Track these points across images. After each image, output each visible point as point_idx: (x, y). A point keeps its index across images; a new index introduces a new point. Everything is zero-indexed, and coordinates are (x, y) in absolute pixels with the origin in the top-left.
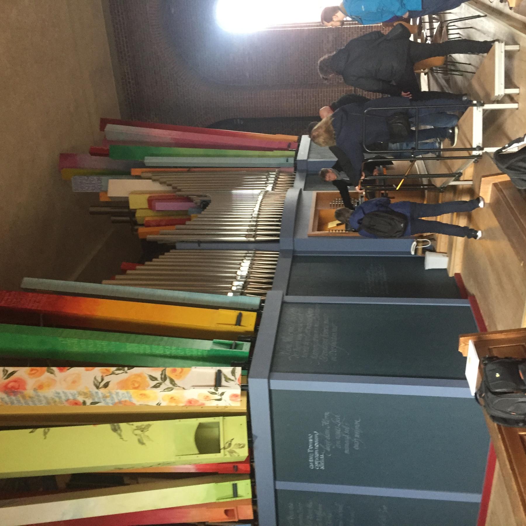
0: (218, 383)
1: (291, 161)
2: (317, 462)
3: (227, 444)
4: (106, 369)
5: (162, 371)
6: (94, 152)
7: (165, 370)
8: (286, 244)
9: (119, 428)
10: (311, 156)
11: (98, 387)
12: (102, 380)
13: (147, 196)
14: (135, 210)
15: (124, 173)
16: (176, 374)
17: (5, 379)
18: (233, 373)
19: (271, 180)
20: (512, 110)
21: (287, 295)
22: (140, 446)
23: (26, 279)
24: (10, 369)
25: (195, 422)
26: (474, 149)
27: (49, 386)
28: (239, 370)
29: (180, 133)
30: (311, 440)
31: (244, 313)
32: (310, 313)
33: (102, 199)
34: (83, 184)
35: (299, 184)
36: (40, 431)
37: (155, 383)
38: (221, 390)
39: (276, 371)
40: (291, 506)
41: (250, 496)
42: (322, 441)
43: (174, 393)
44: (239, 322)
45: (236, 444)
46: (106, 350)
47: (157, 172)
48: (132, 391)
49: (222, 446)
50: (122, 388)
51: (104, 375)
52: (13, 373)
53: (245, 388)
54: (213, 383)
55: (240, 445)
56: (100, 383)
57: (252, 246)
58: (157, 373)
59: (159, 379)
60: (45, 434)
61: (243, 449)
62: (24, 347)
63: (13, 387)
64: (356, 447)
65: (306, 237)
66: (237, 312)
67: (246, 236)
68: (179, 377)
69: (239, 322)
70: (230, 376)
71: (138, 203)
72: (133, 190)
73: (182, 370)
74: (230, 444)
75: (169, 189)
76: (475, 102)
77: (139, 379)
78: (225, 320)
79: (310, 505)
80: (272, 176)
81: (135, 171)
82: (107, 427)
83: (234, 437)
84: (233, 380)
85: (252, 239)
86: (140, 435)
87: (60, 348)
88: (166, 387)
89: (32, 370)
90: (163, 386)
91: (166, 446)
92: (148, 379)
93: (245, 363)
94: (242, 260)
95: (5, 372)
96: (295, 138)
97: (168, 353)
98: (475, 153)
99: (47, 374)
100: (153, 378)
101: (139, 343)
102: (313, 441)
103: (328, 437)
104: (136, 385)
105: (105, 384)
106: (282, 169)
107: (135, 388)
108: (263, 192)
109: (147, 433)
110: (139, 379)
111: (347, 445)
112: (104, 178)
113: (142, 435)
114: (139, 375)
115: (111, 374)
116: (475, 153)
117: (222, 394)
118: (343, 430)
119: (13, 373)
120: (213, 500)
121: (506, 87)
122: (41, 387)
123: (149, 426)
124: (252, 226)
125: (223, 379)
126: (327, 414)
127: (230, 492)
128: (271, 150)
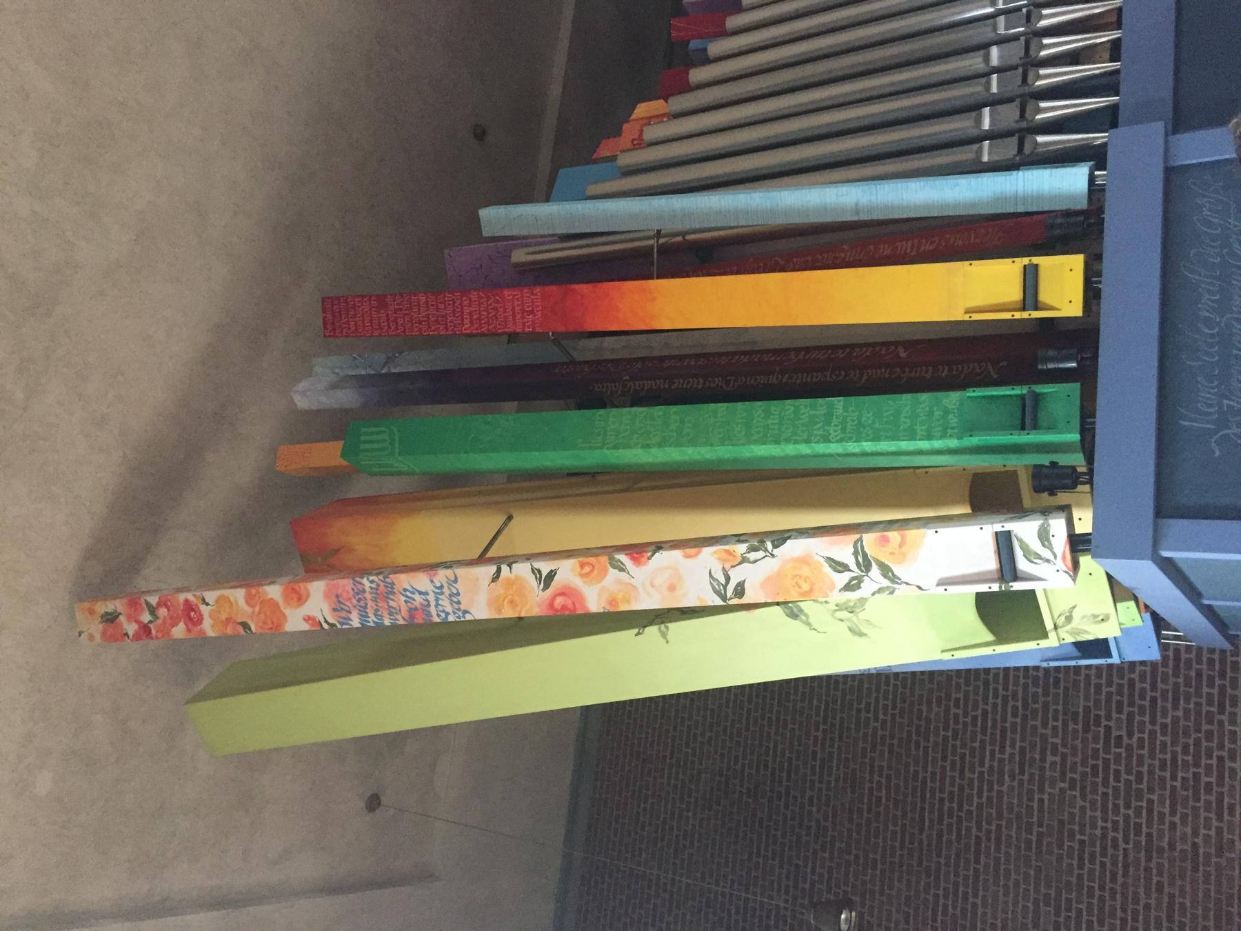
3: (1063, 619)
4: (727, 551)
5: (855, 546)
7: (861, 540)
9: (801, 611)
12: (728, 579)
16: (889, 549)
17: (544, 590)
18: (1044, 536)
21: (1175, 131)
22: (856, 638)
23: (486, 213)
37: (847, 576)
44: (1030, 296)
45: (1084, 617)
51: (727, 566)
52: (551, 575)
55: (1095, 616)
56: (725, 587)
58: (843, 549)
59: (853, 566)
60: (664, 635)
61: (1104, 624)
68: (902, 557)
73: (903, 538)
74: (1069, 619)
77: (805, 571)
84: (1048, 561)
86: (850, 620)
88: (876, 587)
92: (827, 569)
95: (537, 572)
99: (613, 573)
100: (840, 567)
104: (806, 587)
105: (736, 589)
109: (862, 615)
110: (805, 571)
113: (854, 619)
114: (804, 560)
115: (740, 563)
119: (551, 575)
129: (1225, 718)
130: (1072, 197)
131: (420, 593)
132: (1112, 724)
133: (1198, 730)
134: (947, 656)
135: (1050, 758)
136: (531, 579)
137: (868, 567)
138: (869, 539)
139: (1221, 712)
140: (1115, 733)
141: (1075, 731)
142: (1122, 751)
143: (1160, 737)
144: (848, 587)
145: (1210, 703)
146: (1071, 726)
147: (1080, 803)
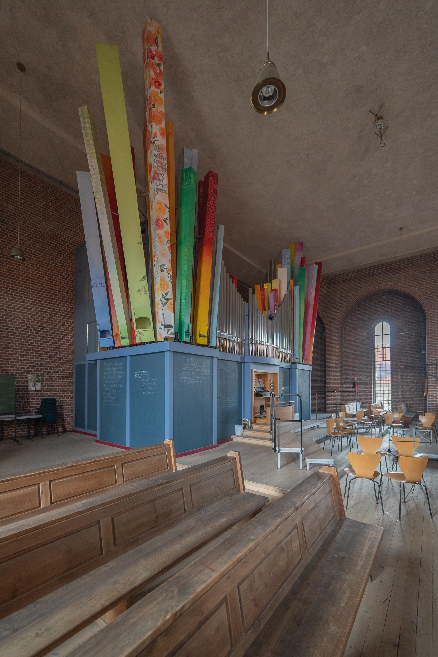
0: (165, 326)
1: (297, 361)
2: (138, 375)
6: (303, 260)
8: (248, 359)
10: (300, 371)
11: (161, 266)
12: (165, 269)
13: (278, 288)
14: (271, 283)
15: (292, 276)
18: (171, 333)
19: (286, 351)
20: (299, 466)
22: (137, 290)
23: (223, 226)
24: (168, 221)
25: (150, 316)
26: (279, 448)
27: (160, 242)
28: (173, 336)
29: (313, 303)
30: (146, 372)
31: (206, 338)
32: (208, 371)
33: (277, 265)
34: (286, 255)
35: (284, 365)
36: (141, 240)
38: (163, 328)
39: (174, 354)
40: (121, 364)
41: (123, 345)
42: (146, 377)
43: (161, 306)
44: (201, 336)
46: (183, 270)
47: (291, 293)
48: (160, 284)
49: (140, 330)
50: (161, 279)
52: (166, 222)
53: (165, 339)
54: (166, 324)
57: (247, 342)
59: (167, 297)
60: (140, 243)
62: (183, 228)
63: (159, 223)
64: (144, 393)
65: (251, 369)
66: (206, 335)
67: (252, 339)
69: (201, 336)
70: (170, 332)
71: (275, 284)
72: (282, 281)
74: (141, 334)
75: (282, 300)
76: (303, 449)
77: (166, 287)
78: (202, 328)
79: (122, 372)
80: (288, 351)
81: (292, 282)
82: (145, 274)
83: (145, 335)
85: (250, 342)
87: (183, 246)
89: (168, 232)
90: (163, 299)
91: (140, 304)
92: (166, 291)
93: (178, 338)
94: (239, 337)
95: (167, 219)
96: (311, 363)
97: (182, 301)
98: (277, 448)
99: (167, 240)
100: (167, 294)
101: (187, 286)
102: (146, 373)
103: (148, 380)
104: (163, 286)
106: (292, 357)
107: (161, 285)
108: (277, 347)
109: (143, 293)
110: (166, 287)
111: (145, 388)
112: (289, 266)
114: (168, 287)
116: (277, 448)
117: (161, 329)
118: (150, 386)
119: (166, 222)
120: (120, 328)
121: (310, 464)
122: (160, 238)
123: (147, 294)
124: (257, 342)
125: (168, 329)
126: (156, 379)
127: (123, 336)
128: (304, 351)
129: (46, 357)
130: (211, 344)
131: (163, 179)
132: (42, 332)
133: (42, 351)
134: (132, 309)
135: (30, 316)
136: (165, 217)
137: (166, 300)
138: (171, 301)
139: (48, 357)
140: (39, 333)
141: (39, 323)
142: (34, 334)
143: (39, 343)
144: (163, 295)
145: (50, 354)
146: (40, 322)
147: (18, 322)
